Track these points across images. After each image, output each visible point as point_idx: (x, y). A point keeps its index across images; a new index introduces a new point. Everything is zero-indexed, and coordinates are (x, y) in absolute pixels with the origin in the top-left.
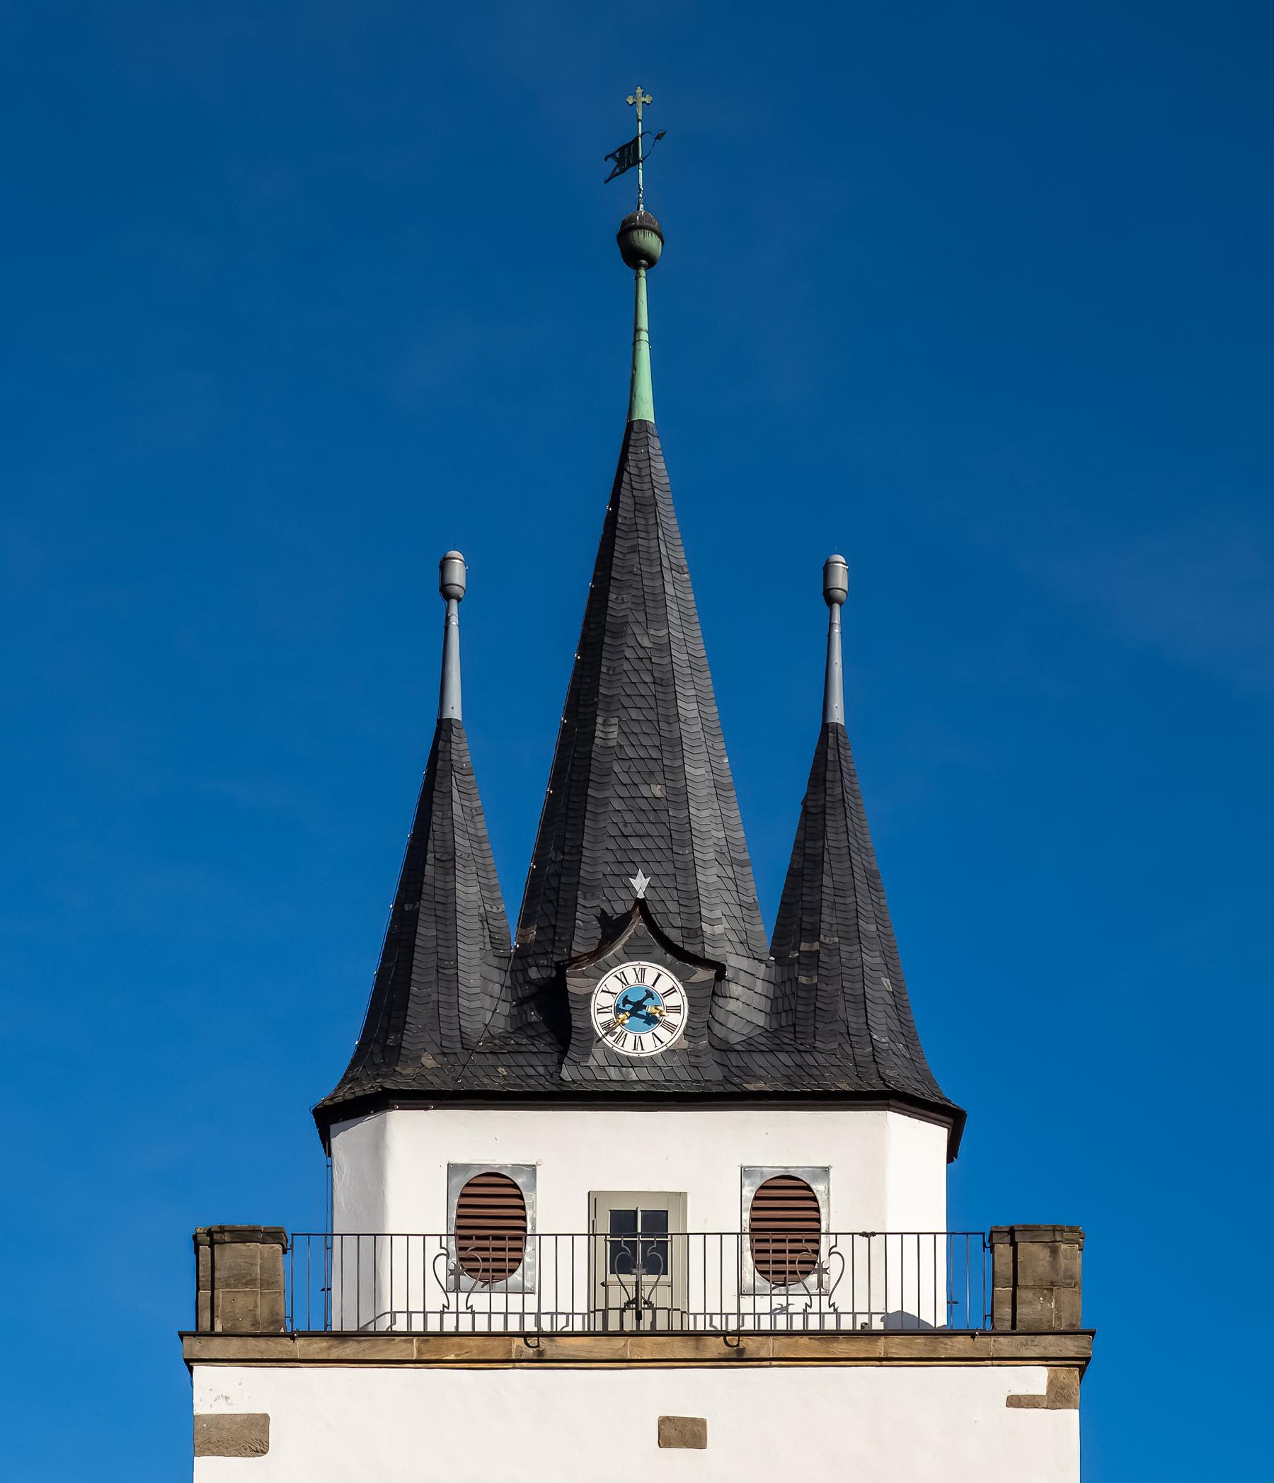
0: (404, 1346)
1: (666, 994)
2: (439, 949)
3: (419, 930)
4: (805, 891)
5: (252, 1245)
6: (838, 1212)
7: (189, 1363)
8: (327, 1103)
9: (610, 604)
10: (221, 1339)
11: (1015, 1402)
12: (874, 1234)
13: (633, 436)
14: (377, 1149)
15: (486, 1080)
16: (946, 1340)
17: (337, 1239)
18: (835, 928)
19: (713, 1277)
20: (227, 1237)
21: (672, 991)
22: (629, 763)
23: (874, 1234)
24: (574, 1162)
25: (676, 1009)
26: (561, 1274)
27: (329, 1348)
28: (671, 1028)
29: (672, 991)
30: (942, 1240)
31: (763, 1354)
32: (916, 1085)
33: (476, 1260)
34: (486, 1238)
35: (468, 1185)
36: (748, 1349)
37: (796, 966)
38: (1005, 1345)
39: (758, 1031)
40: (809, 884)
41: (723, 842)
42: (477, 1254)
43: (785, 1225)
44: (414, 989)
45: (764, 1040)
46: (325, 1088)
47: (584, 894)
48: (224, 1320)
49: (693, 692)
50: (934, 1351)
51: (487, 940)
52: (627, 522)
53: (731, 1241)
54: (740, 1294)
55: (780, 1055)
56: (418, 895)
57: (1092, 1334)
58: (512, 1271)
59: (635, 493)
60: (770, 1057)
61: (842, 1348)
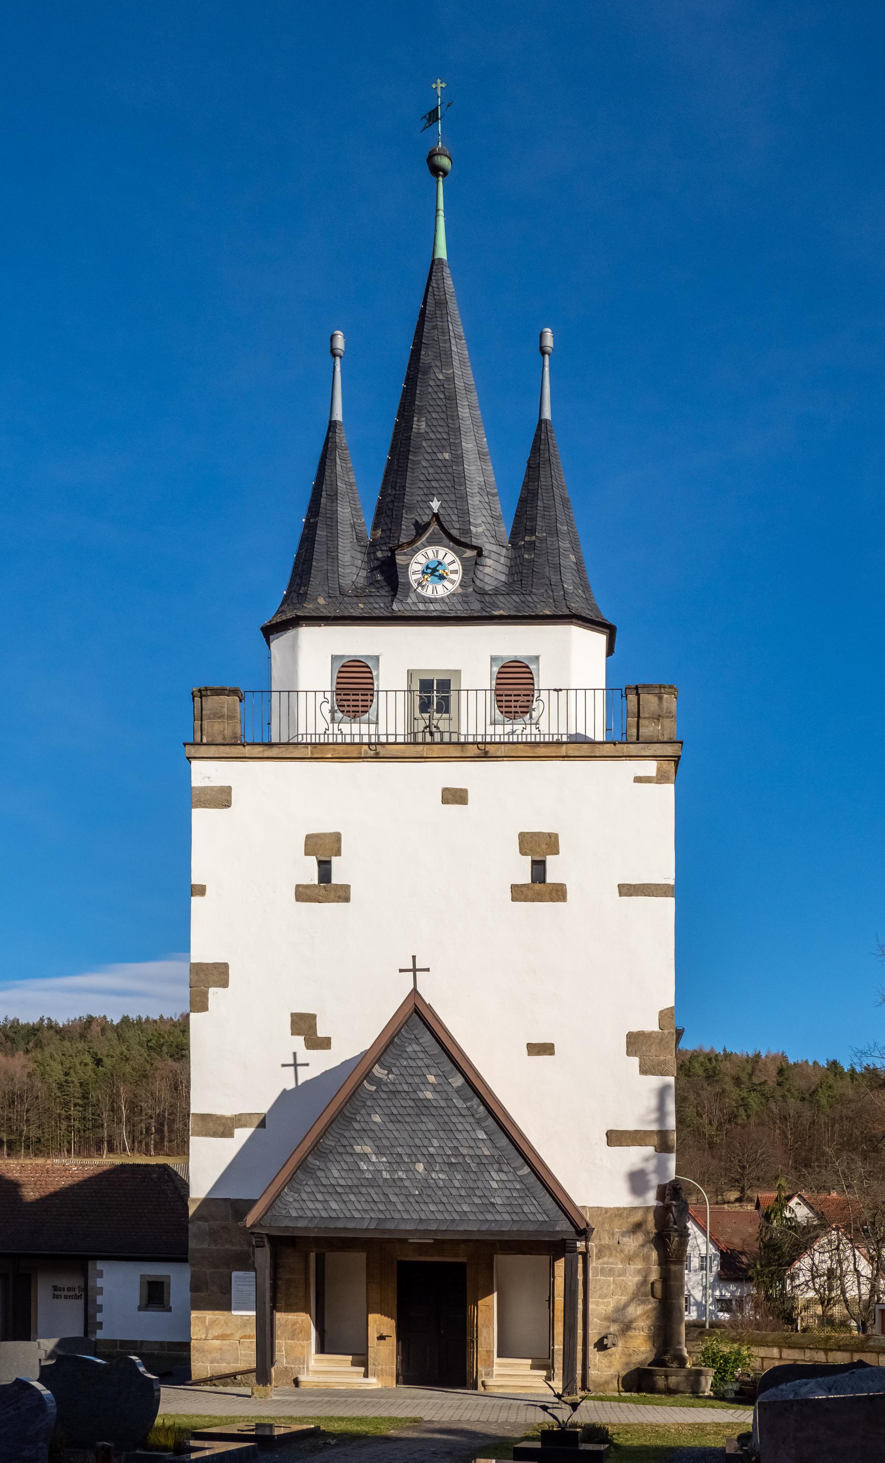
0: (303, 750)
1: (450, 564)
5: (222, 697)
6: (544, 679)
11: (638, 780)
12: (561, 690)
14: (294, 647)
19: (475, 715)
21: (453, 562)
23: (561, 690)
24: (399, 653)
25: (456, 572)
26: (392, 715)
28: (453, 582)
29: (453, 562)
30: (600, 695)
31: (499, 754)
32: (589, 612)
35: (343, 666)
38: (633, 749)
41: (483, 483)
43: (515, 686)
44: (314, 563)
45: (504, 588)
46: (268, 617)
50: (593, 752)
55: (513, 597)
57: (681, 743)
61: (542, 751)
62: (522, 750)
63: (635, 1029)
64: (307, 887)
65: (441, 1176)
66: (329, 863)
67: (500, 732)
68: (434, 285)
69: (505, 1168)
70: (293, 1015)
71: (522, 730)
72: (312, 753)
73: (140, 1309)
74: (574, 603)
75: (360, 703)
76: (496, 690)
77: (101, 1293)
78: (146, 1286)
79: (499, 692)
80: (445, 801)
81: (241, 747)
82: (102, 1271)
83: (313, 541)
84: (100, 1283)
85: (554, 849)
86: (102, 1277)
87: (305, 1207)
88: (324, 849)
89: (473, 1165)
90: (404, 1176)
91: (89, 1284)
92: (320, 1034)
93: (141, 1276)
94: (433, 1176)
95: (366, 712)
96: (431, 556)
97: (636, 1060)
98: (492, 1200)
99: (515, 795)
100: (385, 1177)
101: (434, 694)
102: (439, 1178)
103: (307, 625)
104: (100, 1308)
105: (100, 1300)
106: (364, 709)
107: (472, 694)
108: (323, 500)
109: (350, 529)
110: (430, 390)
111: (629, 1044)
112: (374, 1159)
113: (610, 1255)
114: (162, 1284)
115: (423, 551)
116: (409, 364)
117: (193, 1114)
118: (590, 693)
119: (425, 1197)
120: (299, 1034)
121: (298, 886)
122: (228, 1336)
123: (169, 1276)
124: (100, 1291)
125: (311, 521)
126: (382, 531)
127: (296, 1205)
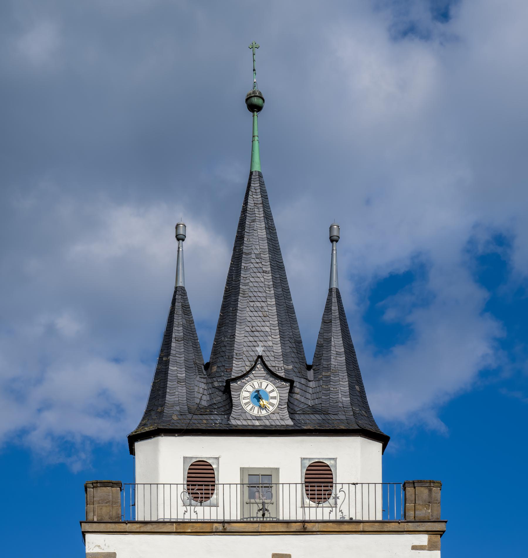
1: (271, 392)
2: (178, 375)
3: (170, 367)
4: (324, 352)
5: (109, 488)
6: (341, 476)
7: (84, 533)
8: (134, 434)
9: (245, 242)
11: (414, 548)
12: (357, 484)
13: (253, 177)
14: (156, 451)
15: (198, 425)
16: (388, 524)
17: (281, 486)
18: (336, 366)
19: (291, 502)
20: (99, 485)
21: (273, 391)
22: (253, 303)
23: (357, 484)
24: (232, 457)
25: (275, 398)
26: (228, 501)
27: (140, 527)
29: (273, 391)
30: (379, 488)
31: (314, 530)
32: (370, 427)
33: (198, 494)
34: (202, 485)
35: (192, 465)
37: (321, 381)
38: (411, 526)
39: (306, 406)
40: (326, 350)
42: (199, 492)
43: (319, 480)
44: (168, 390)
45: (309, 410)
47: (236, 354)
48: (98, 516)
49: (278, 276)
51: (197, 371)
52: (251, 210)
53: (299, 486)
54: (303, 507)
55: (316, 415)
56: (168, 354)
57: (446, 522)
59: (254, 199)
60: (312, 416)
61: (346, 527)
68: (253, 190)
71: (202, 513)
72: (176, 528)
74: (360, 420)
76: (214, 485)
79: (307, 484)
83: (166, 373)
95: (209, 498)
96: (263, 387)
101: (259, 484)
103: (165, 435)
106: (207, 496)
107: (286, 487)
108: (173, 345)
109: (193, 366)
110: (252, 266)
116: (235, 247)
118: (174, 487)
125: (164, 359)
126: (218, 367)
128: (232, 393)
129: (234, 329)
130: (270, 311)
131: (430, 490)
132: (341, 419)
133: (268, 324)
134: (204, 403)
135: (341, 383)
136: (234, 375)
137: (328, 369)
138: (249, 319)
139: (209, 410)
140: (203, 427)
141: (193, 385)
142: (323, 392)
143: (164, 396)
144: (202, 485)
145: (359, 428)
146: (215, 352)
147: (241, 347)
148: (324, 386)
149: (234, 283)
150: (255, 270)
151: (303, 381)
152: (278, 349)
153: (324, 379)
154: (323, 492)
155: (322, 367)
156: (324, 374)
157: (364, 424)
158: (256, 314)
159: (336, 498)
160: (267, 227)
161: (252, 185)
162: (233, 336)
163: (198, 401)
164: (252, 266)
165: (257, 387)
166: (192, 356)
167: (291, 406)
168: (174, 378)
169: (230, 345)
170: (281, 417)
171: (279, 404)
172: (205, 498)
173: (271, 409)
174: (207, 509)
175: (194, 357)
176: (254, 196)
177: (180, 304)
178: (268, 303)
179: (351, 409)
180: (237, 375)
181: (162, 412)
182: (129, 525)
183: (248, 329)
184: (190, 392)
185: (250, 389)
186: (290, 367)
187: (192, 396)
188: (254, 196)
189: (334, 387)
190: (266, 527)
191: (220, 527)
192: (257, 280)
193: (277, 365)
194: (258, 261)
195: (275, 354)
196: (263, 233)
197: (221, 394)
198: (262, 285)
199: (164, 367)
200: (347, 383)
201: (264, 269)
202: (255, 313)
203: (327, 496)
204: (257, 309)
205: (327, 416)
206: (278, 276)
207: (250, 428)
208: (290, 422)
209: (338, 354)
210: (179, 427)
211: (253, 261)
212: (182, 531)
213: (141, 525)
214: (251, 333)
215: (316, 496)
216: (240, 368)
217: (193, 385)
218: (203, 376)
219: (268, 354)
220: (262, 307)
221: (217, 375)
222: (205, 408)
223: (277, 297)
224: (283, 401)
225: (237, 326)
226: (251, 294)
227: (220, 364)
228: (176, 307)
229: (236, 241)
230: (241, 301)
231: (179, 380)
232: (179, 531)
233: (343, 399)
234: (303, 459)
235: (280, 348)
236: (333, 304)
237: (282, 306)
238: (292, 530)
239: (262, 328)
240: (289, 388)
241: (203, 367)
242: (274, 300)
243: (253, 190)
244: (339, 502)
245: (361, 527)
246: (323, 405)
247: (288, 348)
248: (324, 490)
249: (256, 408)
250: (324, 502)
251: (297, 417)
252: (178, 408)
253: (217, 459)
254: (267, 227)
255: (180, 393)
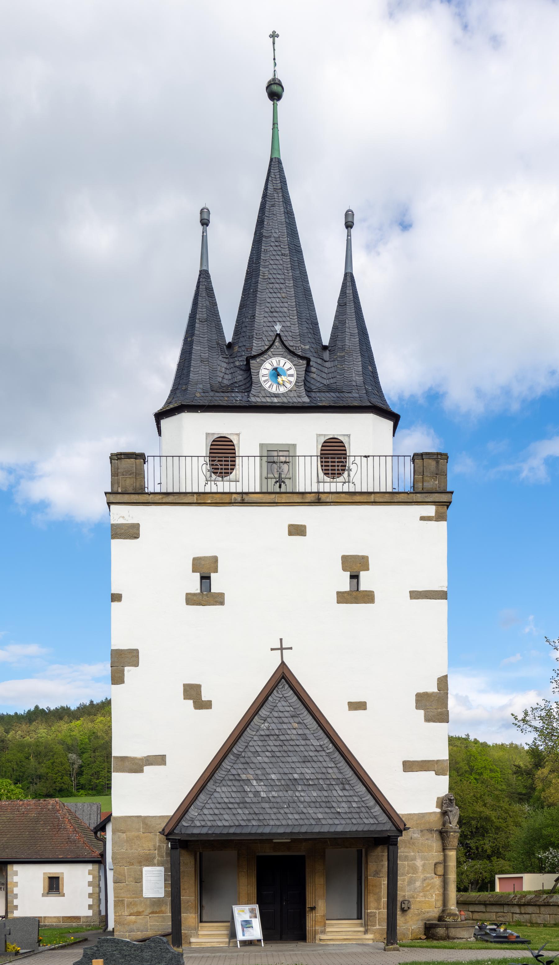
0: (191, 497)
1: (288, 370)
2: (202, 354)
5: (132, 460)
10: (121, 495)
11: (423, 518)
12: (369, 456)
16: (397, 495)
19: (307, 475)
20: (123, 456)
21: (290, 368)
22: (272, 285)
23: (369, 456)
24: (251, 432)
25: (292, 375)
26: (248, 475)
27: (162, 498)
29: (290, 368)
31: (328, 500)
34: (222, 457)
35: (214, 441)
36: (322, 498)
37: (336, 361)
38: (419, 497)
39: (322, 385)
41: (308, 315)
43: (334, 456)
44: (192, 369)
45: (324, 388)
46: (159, 406)
48: (122, 488)
49: (296, 259)
50: (393, 499)
51: (219, 351)
54: (318, 482)
58: (231, 473)
60: (327, 394)
61: (358, 498)
62: (344, 498)
63: (421, 691)
64: (194, 595)
65: (302, 794)
66: (209, 578)
67: (212, 487)
68: (273, 176)
69: (347, 787)
70: (185, 685)
71: (223, 486)
72: (197, 499)
73: (43, 895)
75: (330, 464)
76: (235, 457)
77: (17, 886)
78: (47, 880)
80: (290, 534)
81: (147, 496)
82: (17, 871)
83: (190, 353)
84: (15, 879)
85: (366, 568)
86: (17, 875)
87: (206, 819)
88: (205, 569)
89: (324, 786)
90: (276, 795)
91: (9, 880)
92: (204, 698)
93: (44, 873)
94: (297, 794)
96: (281, 365)
97: (422, 712)
98: (339, 810)
99: (339, 529)
100: (262, 796)
101: (276, 459)
102: (301, 796)
104: (16, 896)
105: (16, 890)
108: (197, 325)
109: (216, 346)
110: (271, 249)
111: (417, 701)
112: (254, 783)
113: (405, 847)
114: (58, 878)
115: (269, 361)
116: (256, 231)
117: (114, 757)
119: (291, 809)
120: (190, 699)
121: (187, 594)
122: (140, 912)
123: (63, 873)
124: (16, 885)
127: (199, 818)
128: (252, 370)
129: (254, 310)
130: (288, 293)
131: (437, 462)
132: (354, 398)
133: (286, 305)
134: (226, 382)
135: (355, 362)
136: (254, 353)
137: (343, 349)
138: (268, 300)
139: (229, 389)
140: (224, 403)
141: (216, 364)
142: (338, 371)
143: (188, 375)
144: (222, 457)
145: (371, 405)
146: (237, 332)
147: (260, 327)
148: (339, 366)
149: (254, 265)
150: (274, 253)
151: (319, 361)
152: (296, 329)
153: (338, 359)
154: (336, 468)
155: (337, 348)
156: (338, 354)
157: (376, 401)
158: (275, 295)
159: (349, 470)
160: (286, 211)
161: (272, 171)
162: (254, 316)
163: (220, 380)
164: (271, 249)
165: (275, 365)
166: (215, 337)
167: (306, 382)
168: (198, 357)
169: (250, 326)
170: (298, 394)
171: (296, 382)
172: (225, 473)
173: (289, 386)
174: (226, 484)
175: (217, 338)
176: (274, 182)
177: (204, 287)
178: (287, 284)
179: (364, 387)
180: (256, 354)
181: (186, 389)
182: (151, 496)
183: (267, 310)
184: (212, 371)
185: (270, 367)
186: (307, 347)
187: (215, 375)
188: (274, 182)
189: (348, 366)
190: (282, 498)
191: (239, 498)
192: (277, 262)
193: (295, 345)
194: (277, 244)
195: (293, 334)
196: (282, 218)
197: (242, 372)
198: (281, 267)
199: (189, 347)
200: (360, 363)
201: (283, 252)
202: (274, 294)
203: (341, 472)
204: (276, 291)
205: (341, 394)
206: (296, 259)
207: (268, 404)
208: (307, 400)
209: (352, 335)
210: (202, 403)
211: (272, 244)
212: (202, 502)
213: (163, 496)
214: (271, 314)
215: (330, 472)
216: (260, 348)
217: (216, 364)
218: (225, 356)
219: (286, 333)
220: (281, 289)
221: (239, 354)
222: (228, 386)
223: (295, 279)
224: (299, 379)
225: (257, 307)
226: (270, 276)
227: (240, 344)
228: (200, 290)
229: (256, 226)
230: (261, 283)
231: (202, 359)
232: (199, 501)
233: (357, 378)
234: (319, 436)
235: (298, 328)
236: (348, 288)
237: (300, 288)
238: (307, 501)
239: (281, 309)
240: (305, 365)
241: (225, 347)
242: (292, 282)
243: (273, 176)
244: (352, 474)
245: (372, 498)
246: (337, 384)
247: (305, 328)
248: (338, 462)
249: (275, 386)
250: (338, 477)
251: (313, 395)
252: (201, 386)
253: (238, 435)
254: (286, 211)
255: (203, 372)
